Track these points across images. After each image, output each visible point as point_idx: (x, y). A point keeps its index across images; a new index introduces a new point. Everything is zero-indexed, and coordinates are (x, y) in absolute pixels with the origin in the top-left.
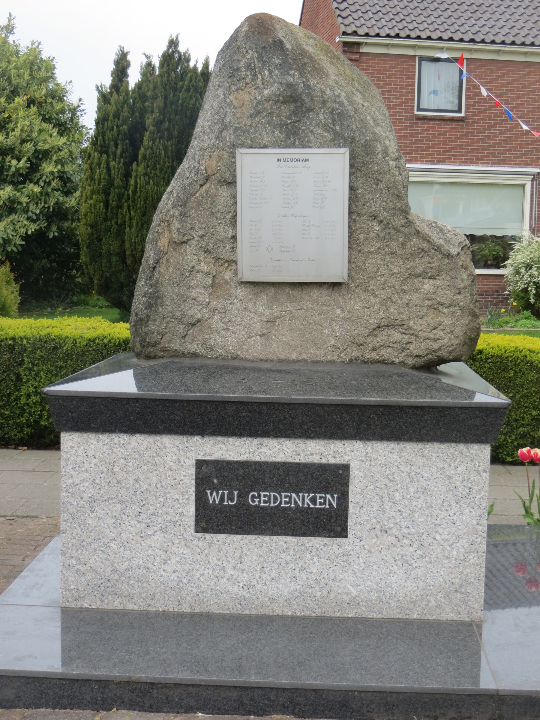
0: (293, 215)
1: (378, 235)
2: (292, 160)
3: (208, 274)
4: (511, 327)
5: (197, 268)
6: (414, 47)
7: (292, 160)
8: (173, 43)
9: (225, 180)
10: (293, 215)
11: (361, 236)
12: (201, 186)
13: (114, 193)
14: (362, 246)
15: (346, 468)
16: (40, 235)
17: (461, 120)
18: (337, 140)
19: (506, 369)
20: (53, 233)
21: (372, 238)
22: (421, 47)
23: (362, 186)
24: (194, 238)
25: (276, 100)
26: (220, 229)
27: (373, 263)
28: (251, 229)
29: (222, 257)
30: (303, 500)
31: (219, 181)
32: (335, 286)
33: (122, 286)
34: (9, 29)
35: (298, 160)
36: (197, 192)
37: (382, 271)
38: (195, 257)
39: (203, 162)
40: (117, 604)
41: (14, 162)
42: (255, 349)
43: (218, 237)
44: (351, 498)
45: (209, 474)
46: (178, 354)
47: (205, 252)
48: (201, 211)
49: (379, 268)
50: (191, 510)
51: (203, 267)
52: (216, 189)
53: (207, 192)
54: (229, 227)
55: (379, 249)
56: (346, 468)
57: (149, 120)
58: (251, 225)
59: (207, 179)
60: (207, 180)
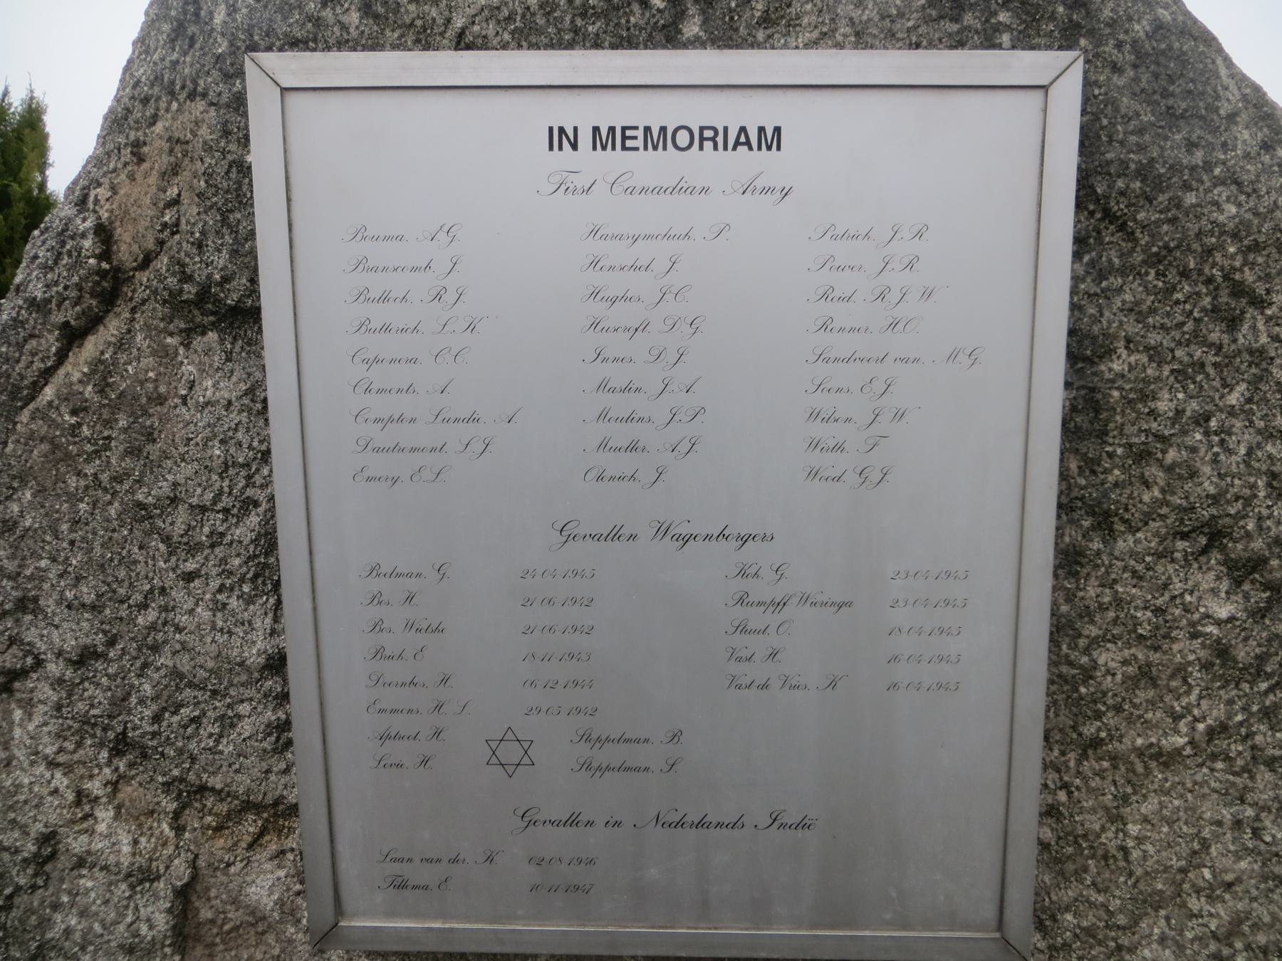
0: (663, 531)
1: (1222, 651)
2: (658, 139)
3: (143, 877)
5: (77, 844)
7: (658, 139)
9: (204, 294)
10: (663, 531)
11: (1107, 657)
12: (72, 337)
14: (1111, 719)
21: (1181, 671)
23: (1132, 328)
24: (39, 663)
26: (193, 610)
28: (377, 626)
29: (217, 782)
31: (175, 304)
34: (6, 93)
35: (706, 137)
36: (47, 374)
37: (1226, 859)
38: (60, 780)
39: (103, 192)
43: (184, 664)
47: (117, 752)
48: (74, 499)
49: (1205, 845)
51: (110, 836)
52: (165, 354)
53: (102, 373)
54: (250, 601)
55: (1221, 729)
58: (376, 599)
59: (109, 288)
60: (109, 299)
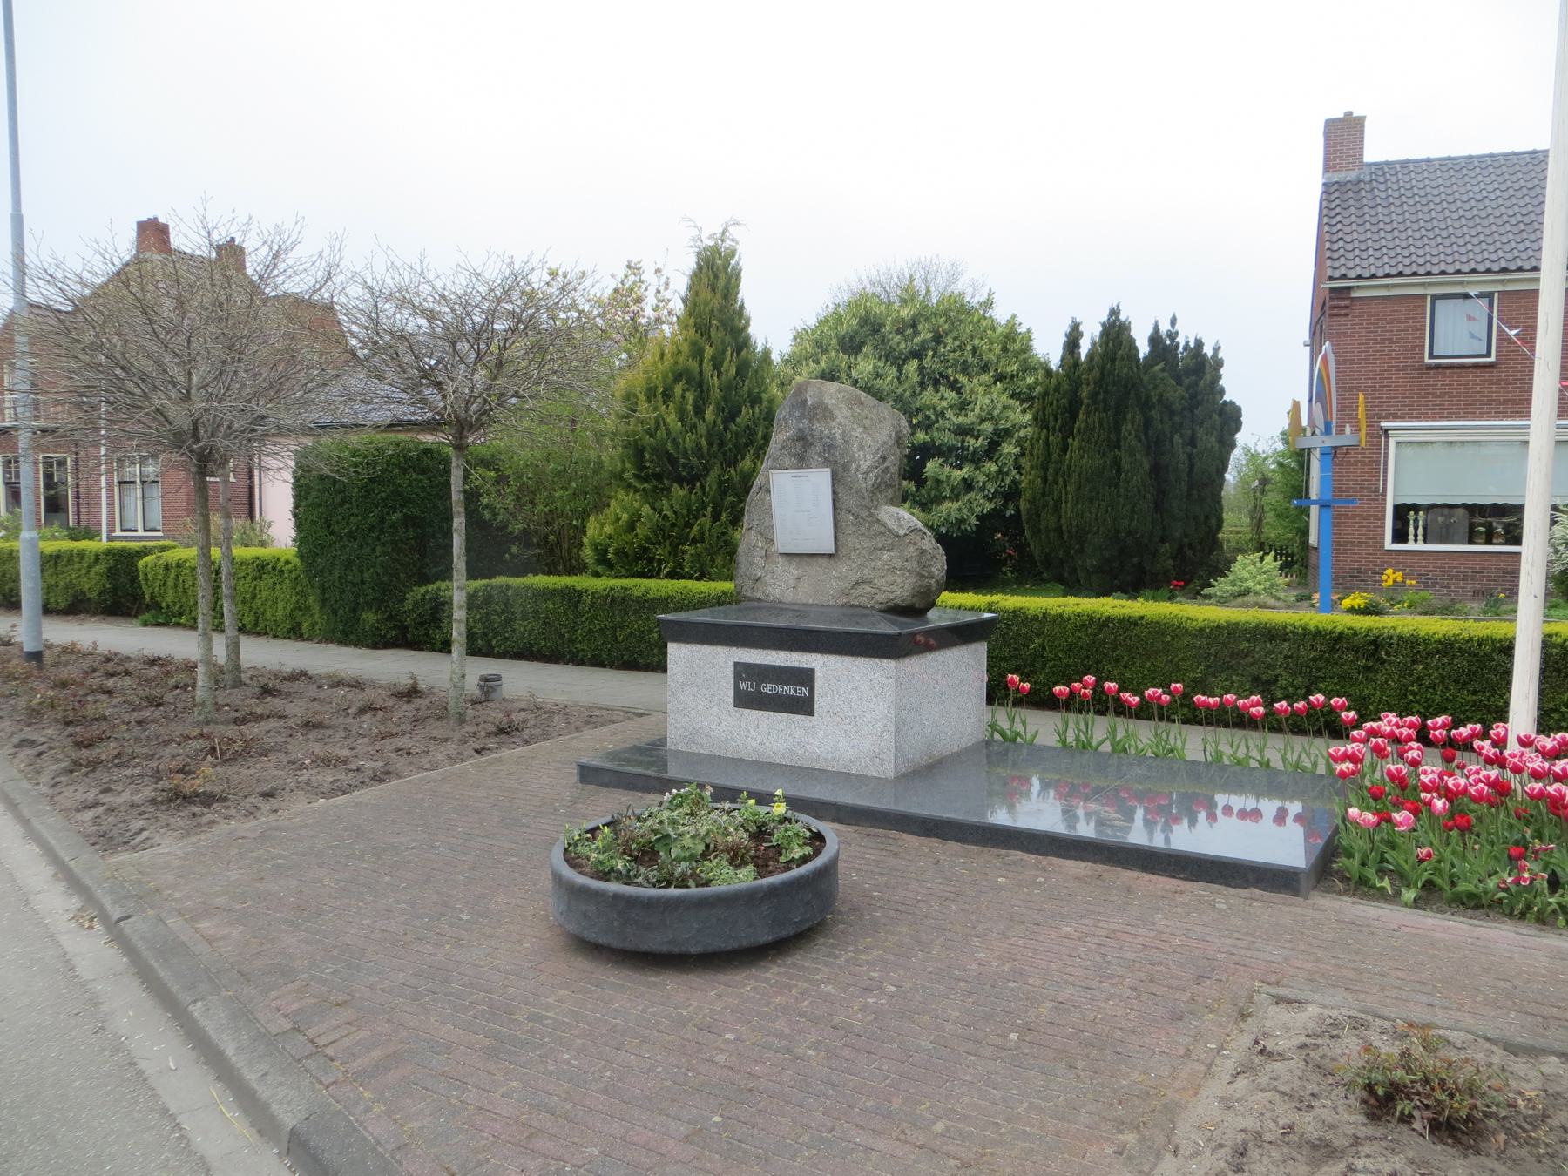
4: (1366, 611)
6: (1422, 285)
8: (1114, 312)
13: (1051, 467)
15: (812, 671)
16: (996, 514)
17: (1491, 366)
18: (826, 462)
19: (1164, 634)
20: (1010, 512)
22: (1430, 284)
25: (792, 439)
27: (851, 541)
30: (789, 690)
32: (830, 555)
33: (1062, 562)
40: (695, 749)
41: (972, 441)
42: (789, 597)
44: (817, 691)
45: (742, 671)
46: (751, 599)
50: (731, 693)
56: (812, 671)
57: (1084, 393)
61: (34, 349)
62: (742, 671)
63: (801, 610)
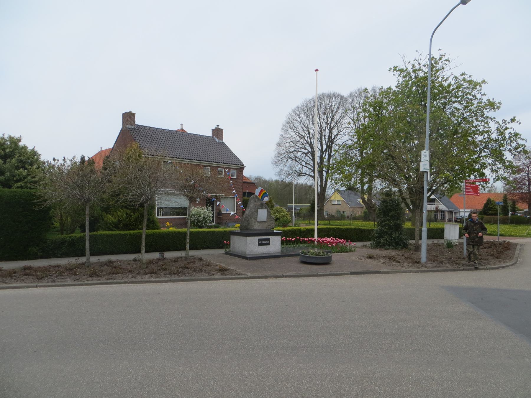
42: (258, 228)
45: (259, 240)
61: (86, 163)
62: (259, 240)
63: (260, 230)
